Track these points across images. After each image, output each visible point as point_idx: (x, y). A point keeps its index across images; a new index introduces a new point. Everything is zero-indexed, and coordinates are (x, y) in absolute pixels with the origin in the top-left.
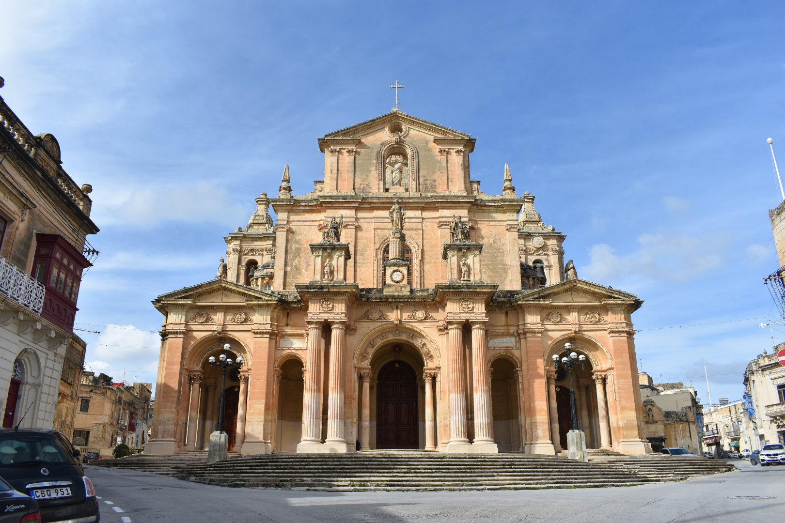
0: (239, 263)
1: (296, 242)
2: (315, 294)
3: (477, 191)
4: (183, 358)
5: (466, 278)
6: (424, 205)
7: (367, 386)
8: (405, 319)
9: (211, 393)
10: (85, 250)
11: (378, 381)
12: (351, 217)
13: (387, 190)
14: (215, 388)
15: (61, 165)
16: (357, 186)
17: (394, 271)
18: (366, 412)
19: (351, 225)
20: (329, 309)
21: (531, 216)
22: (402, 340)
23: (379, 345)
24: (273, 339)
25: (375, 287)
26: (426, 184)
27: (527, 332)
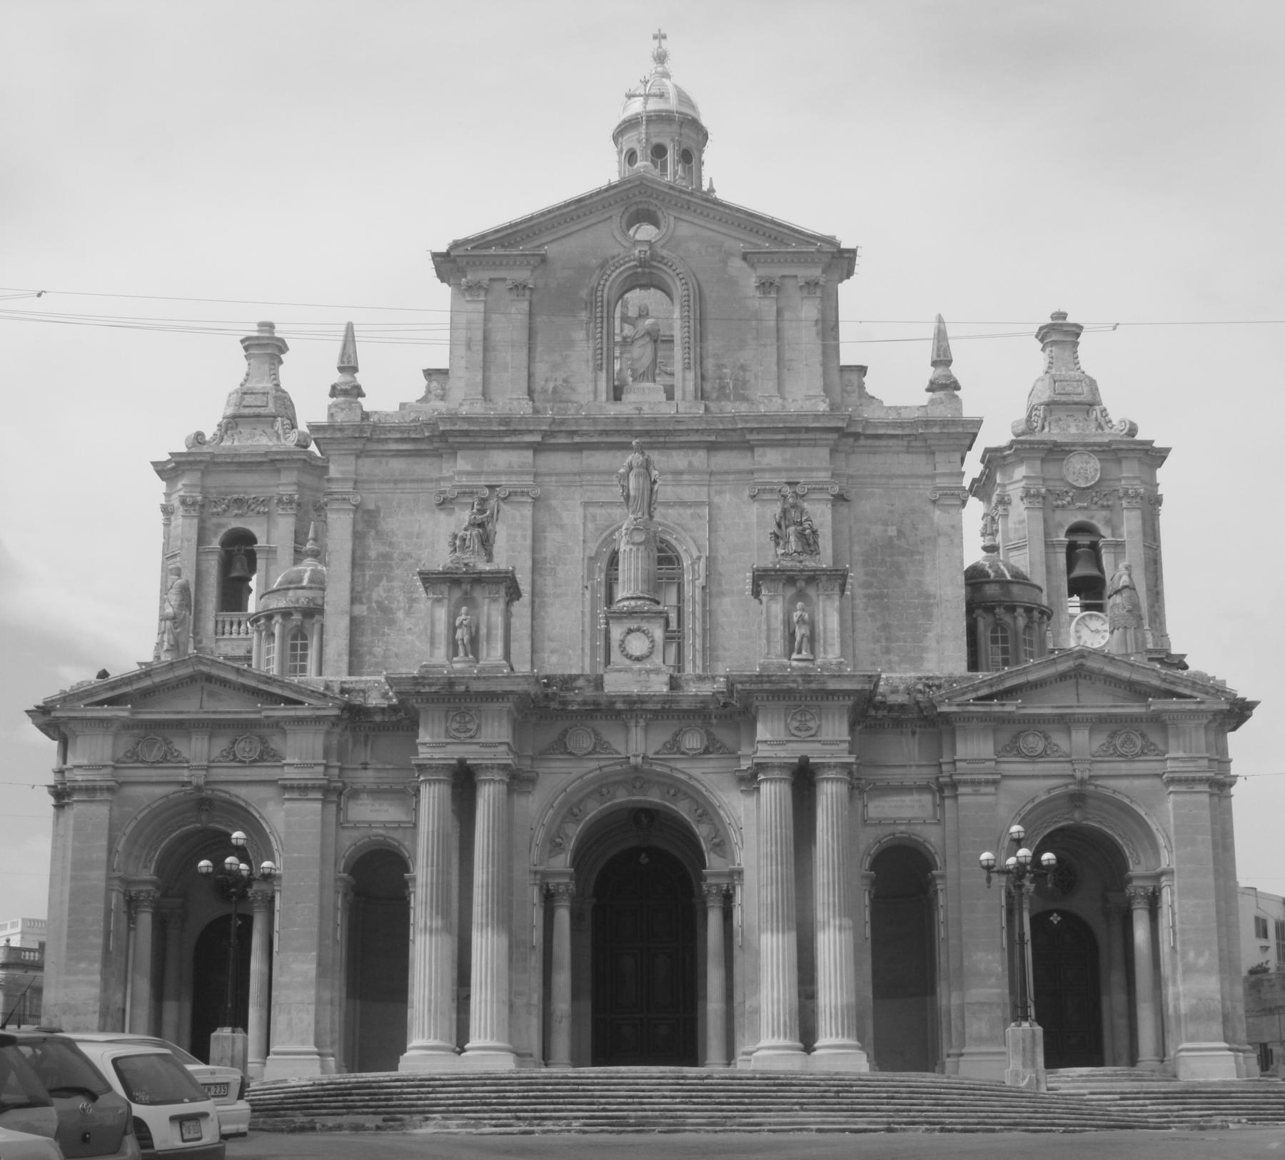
0: (202, 539)
2: (434, 698)
3: (856, 394)
4: (111, 851)
5: (804, 654)
6: (713, 438)
7: (563, 916)
8: (657, 753)
11: (594, 900)
12: (522, 473)
13: (617, 394)
16: (539, 384)
17: (630, 631)
18: (563, 980)
19: (522, 493)
20: (468, 734)
21: (1069, 389)
22: (650, 802)
23: (594, 816)
24: (332, 802)
25: (588, 671)
26: (720, 378)
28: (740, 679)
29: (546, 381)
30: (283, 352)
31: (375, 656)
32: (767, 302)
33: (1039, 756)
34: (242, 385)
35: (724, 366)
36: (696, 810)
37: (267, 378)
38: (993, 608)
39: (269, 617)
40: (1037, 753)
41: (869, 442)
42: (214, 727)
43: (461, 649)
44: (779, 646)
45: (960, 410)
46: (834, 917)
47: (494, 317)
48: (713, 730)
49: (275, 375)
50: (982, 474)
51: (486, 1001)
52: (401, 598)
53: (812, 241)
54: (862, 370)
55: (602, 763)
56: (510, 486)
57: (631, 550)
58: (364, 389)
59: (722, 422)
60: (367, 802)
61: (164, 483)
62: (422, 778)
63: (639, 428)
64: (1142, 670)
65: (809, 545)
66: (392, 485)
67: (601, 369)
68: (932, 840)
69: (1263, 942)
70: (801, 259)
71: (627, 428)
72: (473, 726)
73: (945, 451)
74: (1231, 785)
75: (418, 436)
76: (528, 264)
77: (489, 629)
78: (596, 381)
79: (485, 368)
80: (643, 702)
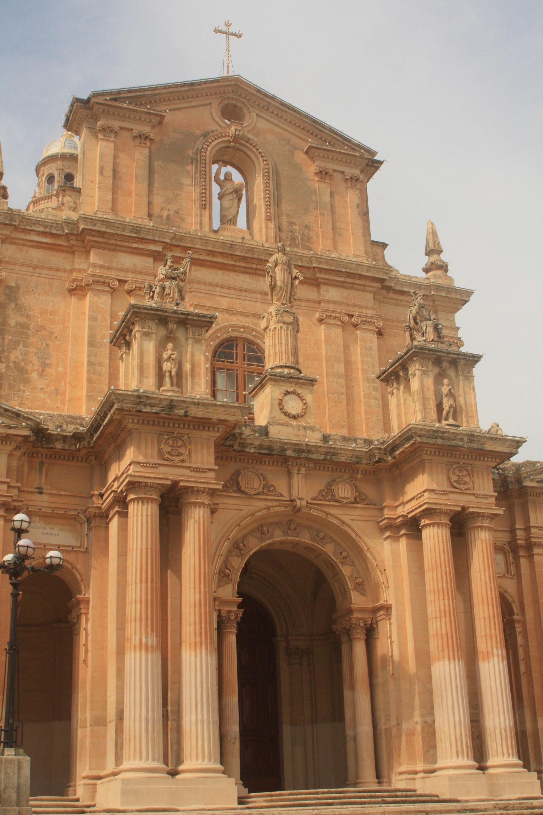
5: (451, 421)
8: (314, 499)
16: (156, 211)
17: (287, 393)
26: (292, 232)
28: (420, 433)
32: (323, 185)
35: (294, 223)
41: (396, 296)
43: (167, 380)
44: (433, 414)
46: (497, 648)
47: (122, 155)
48: (358, 484)
51: (203, 721)
52: (35, 362)
53: (357, 148)
54: (384, 246)
55: (269, 504)
56: (136, 282)
57: (281, 328)
59: (301, 260)
60: (39, 525)
62: (132, 496)
63: (239, 254)
66: (31, 269)
67: (205, 209)
68: (509, 590)
71: (231, 252)
75: (58, 232)
76: (150, 122)
77: (193, 366)
78: (201, 216)
79: (115, 190)
80: (309, 452)
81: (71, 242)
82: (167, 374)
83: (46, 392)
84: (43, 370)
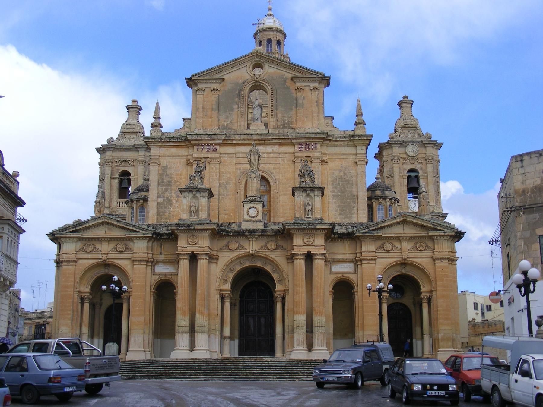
1: (167, 175)
6: (281, 141)
7: (227, 305)
9: (97, 310)
10: (17, 219)
14: (101, 305)
15: (4, 166)
17: (250, 208)
24: (150, 266)
27: (363, 259)
29: (224, 122)
30: (140, 110)
31: (166, 216)
33: (391, 251)
34: (126, 122)
36: (273, 269)
37: (134, 119)
38: (378, 199)
39: (132, 202)
40: (389, 250)
41: (334, 143)
42: (110, 240)
45: (365, 131)
48: (279, 242)
49: (137, 119)
50: (379, 151)
58: (163, 125)
60: (161, 266)
61: (100, 155)
64: (425, 221)
65: (311, 179)
66: (171, 158)
69: (476, 311)
70: (312, 80)
72: (196, 240)
73: (360, 146)
74: (456, 260)
81: (186, 144)
82: (192, 212)
83: (179, 208)
84: (178, 199)
